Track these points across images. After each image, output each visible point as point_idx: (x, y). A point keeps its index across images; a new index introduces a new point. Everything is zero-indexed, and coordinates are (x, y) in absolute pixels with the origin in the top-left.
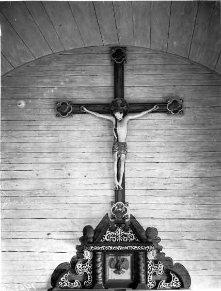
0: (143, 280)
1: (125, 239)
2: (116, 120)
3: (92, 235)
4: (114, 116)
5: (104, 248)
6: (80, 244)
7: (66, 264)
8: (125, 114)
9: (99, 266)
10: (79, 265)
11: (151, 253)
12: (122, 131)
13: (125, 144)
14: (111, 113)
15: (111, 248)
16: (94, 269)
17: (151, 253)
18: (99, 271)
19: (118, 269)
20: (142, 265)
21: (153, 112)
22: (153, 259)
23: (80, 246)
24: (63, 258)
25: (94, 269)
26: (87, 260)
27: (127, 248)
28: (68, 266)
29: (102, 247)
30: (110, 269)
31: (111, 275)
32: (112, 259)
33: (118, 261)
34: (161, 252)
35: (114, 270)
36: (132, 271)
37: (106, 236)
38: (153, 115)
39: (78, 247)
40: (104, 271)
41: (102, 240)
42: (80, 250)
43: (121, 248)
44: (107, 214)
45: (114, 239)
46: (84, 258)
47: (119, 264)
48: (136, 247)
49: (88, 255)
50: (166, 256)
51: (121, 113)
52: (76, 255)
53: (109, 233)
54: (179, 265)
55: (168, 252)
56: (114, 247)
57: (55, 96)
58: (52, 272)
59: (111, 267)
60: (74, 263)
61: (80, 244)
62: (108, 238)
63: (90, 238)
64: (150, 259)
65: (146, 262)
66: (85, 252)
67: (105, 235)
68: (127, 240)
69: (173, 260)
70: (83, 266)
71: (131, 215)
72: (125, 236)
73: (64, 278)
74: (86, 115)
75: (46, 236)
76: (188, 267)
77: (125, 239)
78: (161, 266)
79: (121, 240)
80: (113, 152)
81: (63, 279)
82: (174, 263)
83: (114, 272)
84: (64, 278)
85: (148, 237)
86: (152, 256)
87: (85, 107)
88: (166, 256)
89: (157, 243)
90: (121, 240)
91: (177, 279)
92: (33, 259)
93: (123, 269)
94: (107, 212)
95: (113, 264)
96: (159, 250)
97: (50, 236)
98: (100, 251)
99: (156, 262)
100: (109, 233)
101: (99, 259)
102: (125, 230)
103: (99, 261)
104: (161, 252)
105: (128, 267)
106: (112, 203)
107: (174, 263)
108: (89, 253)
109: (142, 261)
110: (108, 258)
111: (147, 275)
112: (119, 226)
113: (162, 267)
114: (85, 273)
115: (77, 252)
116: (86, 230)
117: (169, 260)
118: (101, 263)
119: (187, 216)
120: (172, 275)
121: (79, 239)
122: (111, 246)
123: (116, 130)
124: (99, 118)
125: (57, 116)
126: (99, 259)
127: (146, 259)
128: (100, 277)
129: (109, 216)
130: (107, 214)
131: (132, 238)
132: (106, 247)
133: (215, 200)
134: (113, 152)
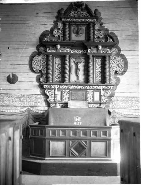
0: (92, 38)
1: (82, 16)
3: (63, 12)
5: (70, 20)
6: (55, 20)
7: (48, 31)
9: (67, 31)
10: (55, 31)
15: (74, 19)
17: (97, 25)
18: (67, 33)
19: (77, 33)
20: (92, 31)
22: (98, 28)
23: (55, 21)
24: (46, 28)
26: (60, 28)
28: (49, 32)
29: (69, 19)
31: (74, 37)
32: (74, 28)
33: (78, 29)
34: (102, 25)
35: (75, 34)
36: (86, 35)
37: (71, 14)
39: (54, 22)
40: (70, 34)
41: (69, 16)
42: (56, 23)
43: (80, 20)
45: (76, 15)
46: (58, 27)
47: (78, 30)
48: (89, 19)
49: (60, 25)
50: (105, 28)
52: (53, 26)
55: (106, 26)
56: (76, 19)
57: (29, 26)
58: (39, 35)
59: (74, 33)
60: (52, 30)
61: (55, 20)
62: (72, 15)
63: (62, 14)
64: (96, 28)
66: (59, 24)
67: (71, 13)
68: (83, 16)
70: (57, 32)
72: (83, 14)
73: (47, 38)
77: (82, 16)
78: (103, 33)
79: (80, 16)
81: (46, 39)
82: (110, 32)
83: (75, 36)
84: (47, 38)
85: (93, 92)
86: (97, 27)
88: (105, 28)
90: (80, 16)
91: (111, 40)
95: (75, 31)
97: (38, 15)
98: (67, 22)
99: (99, 30)
101: (67, 27)
103: (67, 31)
104: (102, 25)
105: (83, 33)
107: (110, 32)
109: (92, 35)
110: (72, 28)
112: (79, 8)
113: (103, 33)
114: (59, 35)
116: (59, 12)
117: (107, 30)
120: (108, 37)
121: (56, 17)
122: (74, 18)
126: (67, 27)
127: (94, 29)
128: (67, 36)
131: (86, 15)
132: (71, 19)
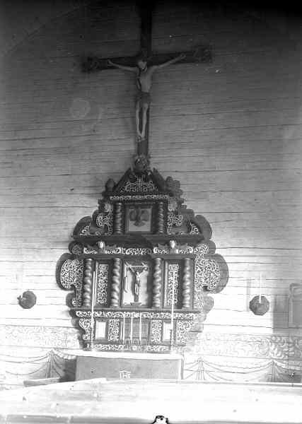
2: (140, 69)
4: (137, 66)
6: (102, 198)
8: (149, 65)
10: (100, 218)
11: (172, 205)
12: (146, 83)
13: (148, 94)
14: (134, 65)
16: (114, 223)
21: (179, 62)
25: (114, 223)
27: (146, 197)
29: (121, 197)
30: (130, 222)
35: (134, 222)
36: (152, 223)
38: (180, 66)
44: (130, 169)
49: (108, 208)
50: (187, 208)
51: (144, 61)
53: (129, 183)
54: (200, 217)
55: (189, 205)
60: (96, 215)
65: (166, 213)
69: (195, 211)
71: (154, 169)
74: (114, 70)
75: (70, 192)
76: (208, 218)
80: (136, 102)
82: (196, 215)
83: (135, 224)
86: (171, 208)
87: (111, 61)
88: (187, 208)
89: (179, 196)
92: (57, 214)
93: (144, 222)
94: (128, 167)
95: (133, 217)
96: (180, 203)
99: (176, 213)
100: (129, 183)
102: (146, 180)
106: (134, 156)
107: (196, 215)
108: (110, 206)
111: (193, 293)
115: (99, 207)
117: (191, 212)
118: (120, 219)
119: (210, 168)
123: (139, 80)
124: (125, 70)
125: (84, 71)
129: (132, 170)
130: (130, 169)
133: (143, 389)
134: (136, 102)
